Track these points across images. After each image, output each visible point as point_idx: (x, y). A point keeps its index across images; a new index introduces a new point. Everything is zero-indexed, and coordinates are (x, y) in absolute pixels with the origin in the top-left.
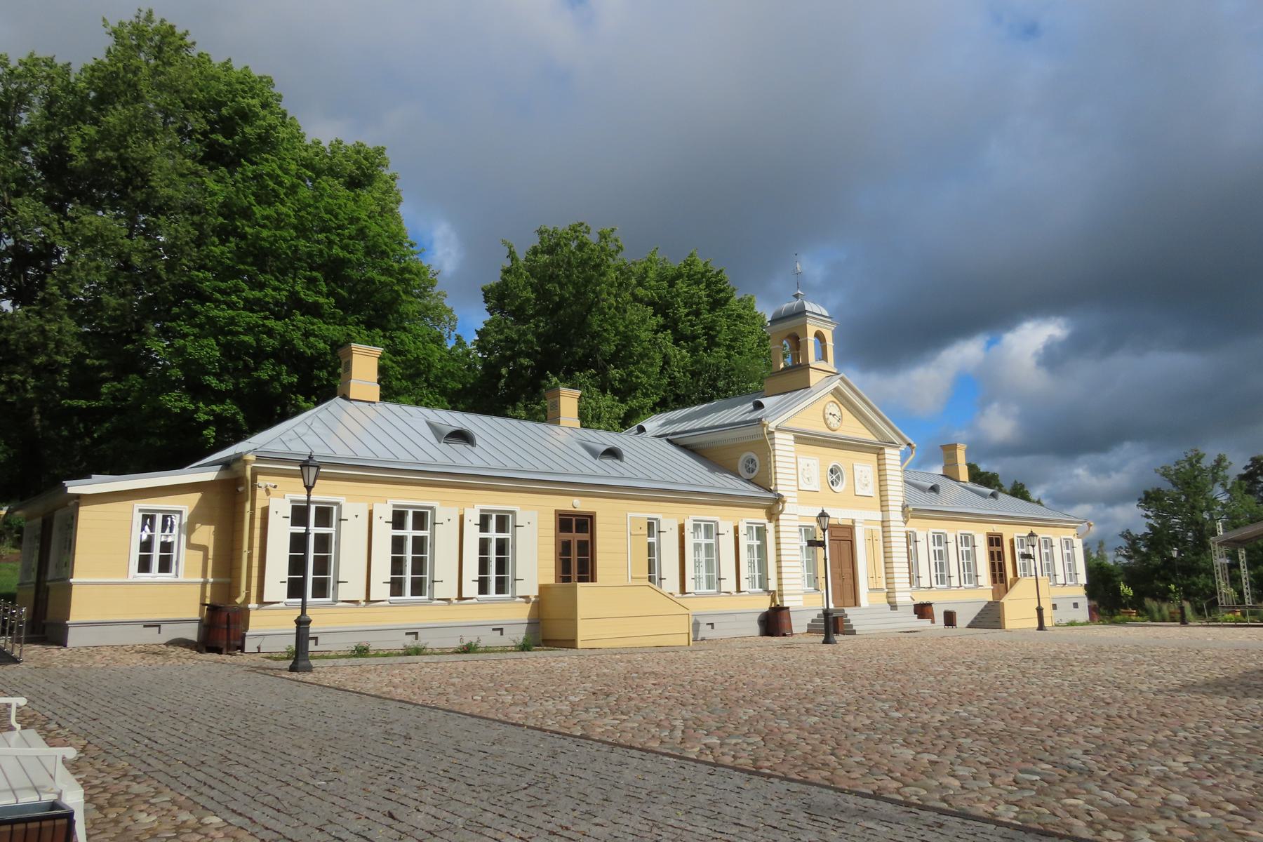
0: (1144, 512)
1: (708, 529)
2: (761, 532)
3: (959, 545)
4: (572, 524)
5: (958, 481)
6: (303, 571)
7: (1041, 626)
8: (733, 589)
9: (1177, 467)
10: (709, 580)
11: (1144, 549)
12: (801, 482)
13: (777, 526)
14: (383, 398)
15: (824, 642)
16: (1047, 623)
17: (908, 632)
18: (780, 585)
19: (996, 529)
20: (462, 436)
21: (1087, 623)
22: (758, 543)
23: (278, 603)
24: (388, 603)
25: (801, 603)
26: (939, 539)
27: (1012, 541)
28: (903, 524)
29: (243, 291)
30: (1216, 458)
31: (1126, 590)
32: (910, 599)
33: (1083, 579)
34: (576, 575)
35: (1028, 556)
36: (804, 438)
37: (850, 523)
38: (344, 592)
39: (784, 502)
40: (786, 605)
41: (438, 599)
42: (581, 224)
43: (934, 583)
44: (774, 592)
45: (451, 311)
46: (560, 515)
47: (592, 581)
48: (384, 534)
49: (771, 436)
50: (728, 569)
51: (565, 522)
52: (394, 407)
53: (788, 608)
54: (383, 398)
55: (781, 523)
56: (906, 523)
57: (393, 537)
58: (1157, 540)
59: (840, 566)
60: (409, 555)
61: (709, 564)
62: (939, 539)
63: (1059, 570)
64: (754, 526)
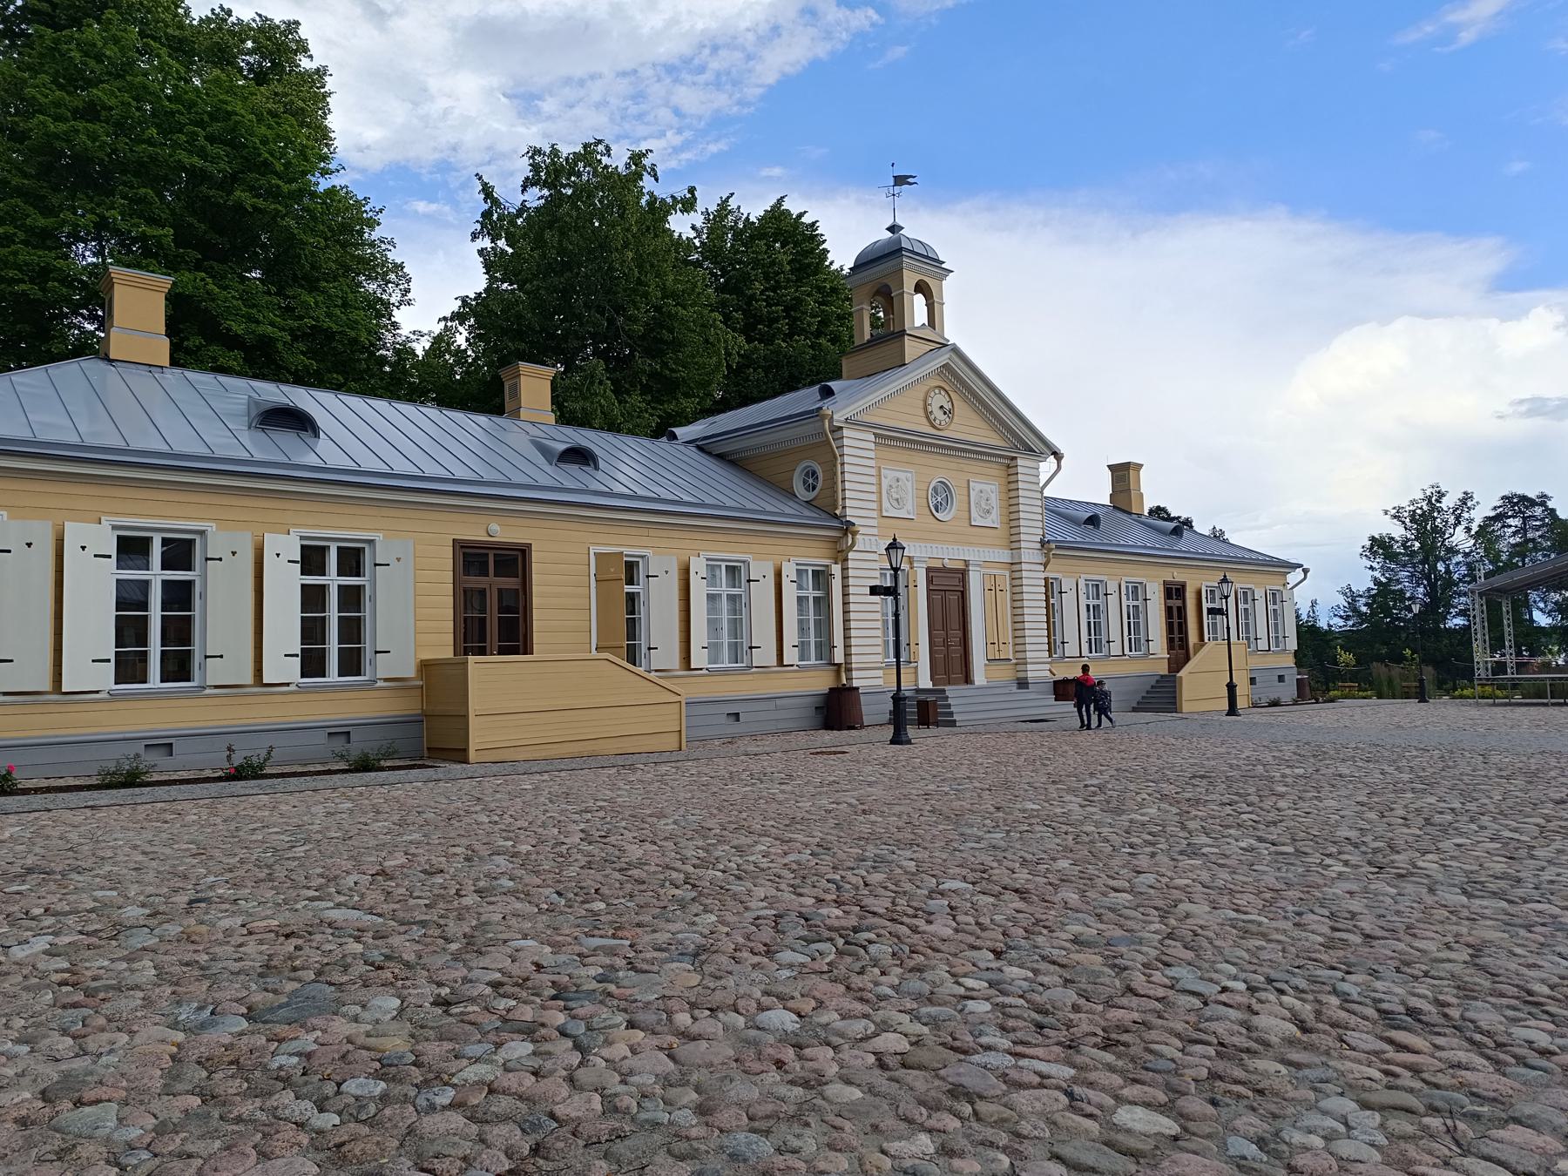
0: (1369, 564)
1: (733, 571)
2: (821, 578)
3: (1124, 597)
4: (486, 563)
5: (1130, 513)
6: (143, 640)
7: (1232, 710)
8: (674, 662)
9: (1412, 508)
10: (735, 649)
11: (1364, 609)
12: (886, 504)
13: (845, 569)
14: (174, 362)
15: (893, 742)
16: (1241, 703)
17: (1031, 721)
18: (847, 655)
19: (1178, 576)
20: (299, 421)
21: (1295, 703)
22: (818, 594)
23: (97, 692)
24: (107, 696)
25: (880, 682)
26: (1097, 588)
27: (1199, 593)
28: (1042, 568)
29: (28, 216)
30: (1461, 496)
31: (1346, 657)
32: (1048, 673)
33: (1292, 644)
34: (496, 644)
35: (1219, 612)
36: (888, 438)
37: (961, 566)
38: (216, 672)
39: (854, 534)
40: (855, 683)
41: (216, 687)
42: (600, 142)
43: (1127, 651)
44: (839, 665)
45: (401, 266)
46: (523, 551)
47: (525, 653)
48: (284, 584)
49: (837, 435)
50: (763, 633)
51: (471, 558)
52: (204, 380)
53: (857, 688)
54: (174, 362)
55: (851, 564)
56: (1045, 566)
57: (303, 586)
58: (1384, 594)
59: (945, 627)
60: (333, 614)
61: (735, 626)
62: (1097, 588)
63: (1262, 632)
64: (810, 569)
